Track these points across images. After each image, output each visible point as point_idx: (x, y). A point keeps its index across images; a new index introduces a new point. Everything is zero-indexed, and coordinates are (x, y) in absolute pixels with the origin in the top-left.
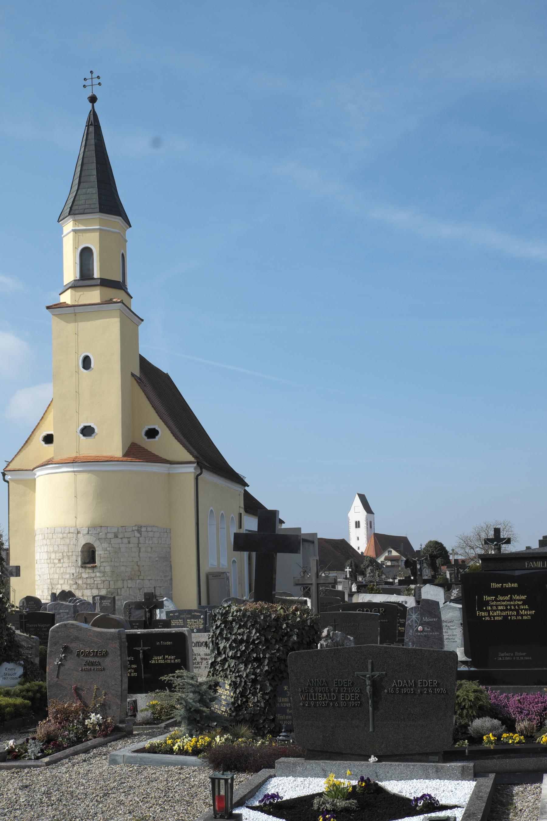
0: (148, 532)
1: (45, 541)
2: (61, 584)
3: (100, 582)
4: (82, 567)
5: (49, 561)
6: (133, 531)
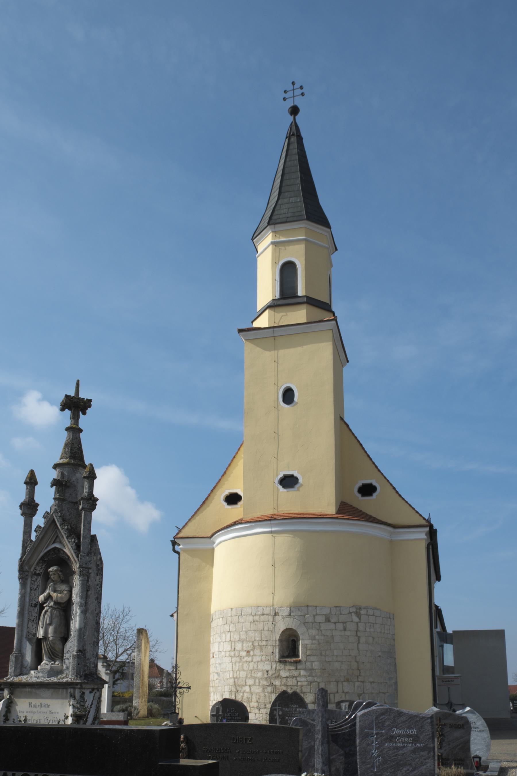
0: (369, 615)
1: (227, 627)
2: (250, 686)
3: (305, 683)
4: (280, 662)
5: (232, 653)
6: (350, 613)
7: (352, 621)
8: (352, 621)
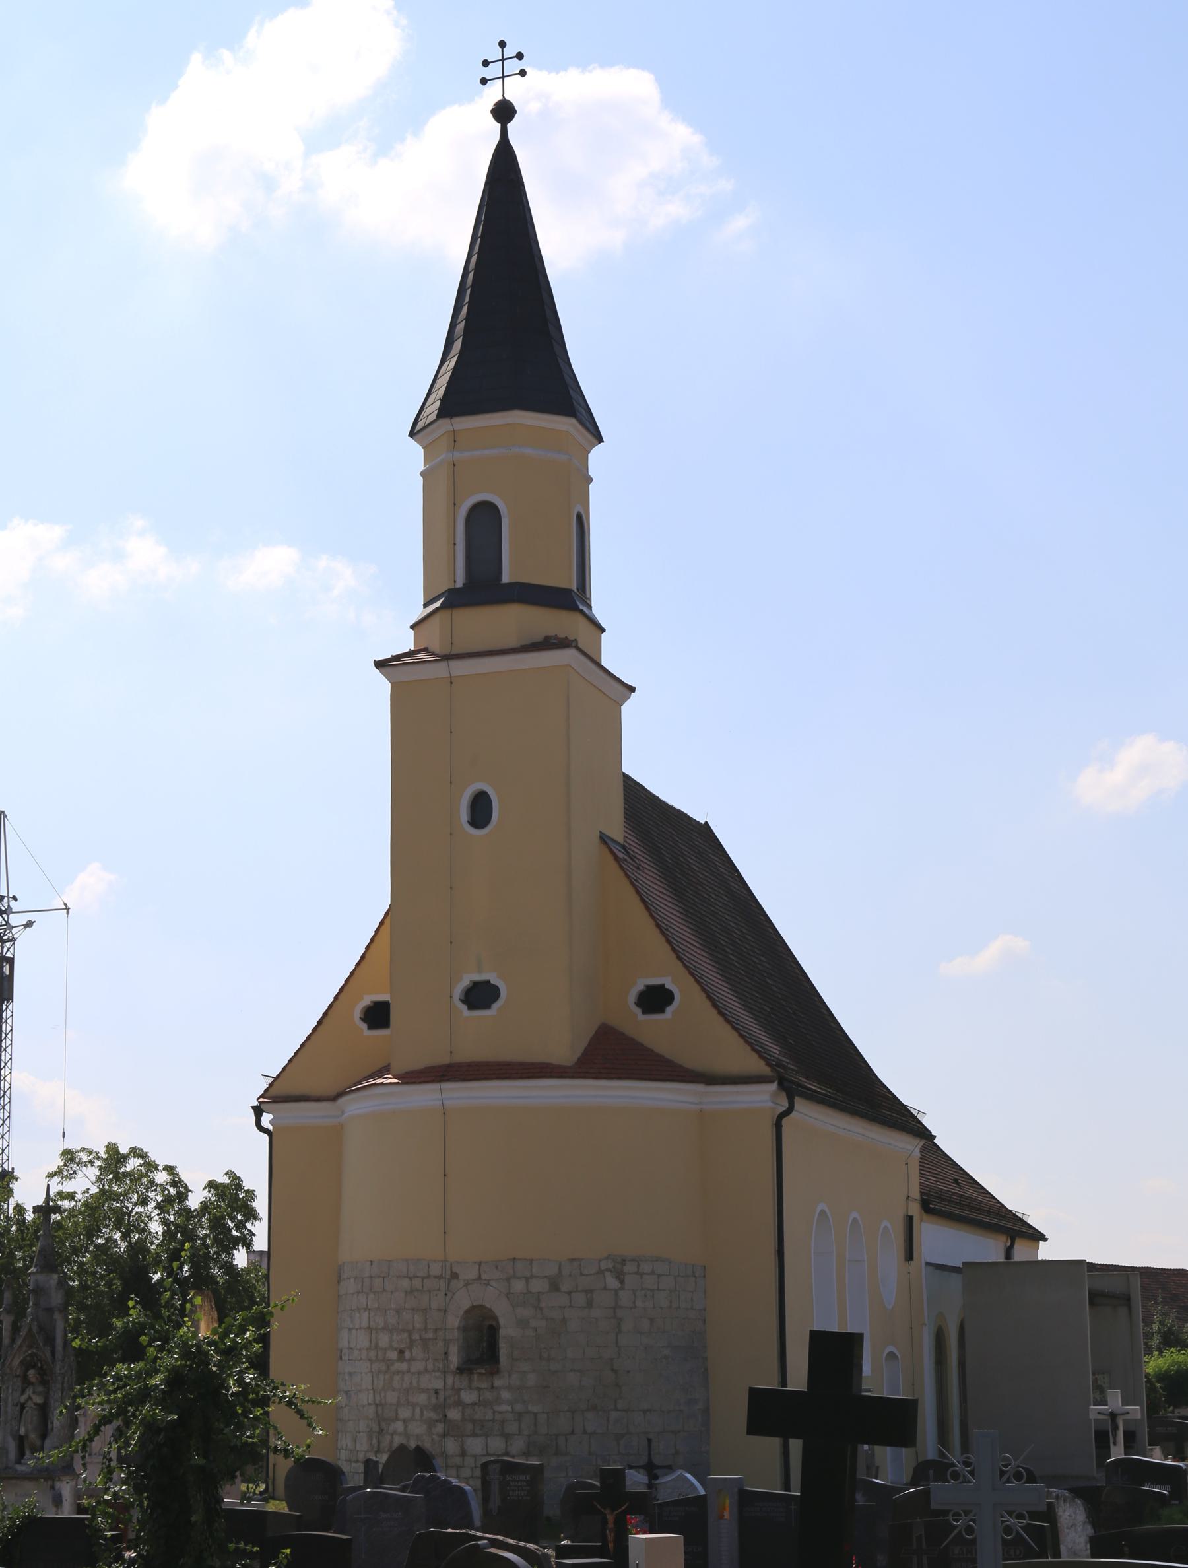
0: (642, 1275)
6: (601, 1272)
7: (605, 1288)
8: (605, 1288)
